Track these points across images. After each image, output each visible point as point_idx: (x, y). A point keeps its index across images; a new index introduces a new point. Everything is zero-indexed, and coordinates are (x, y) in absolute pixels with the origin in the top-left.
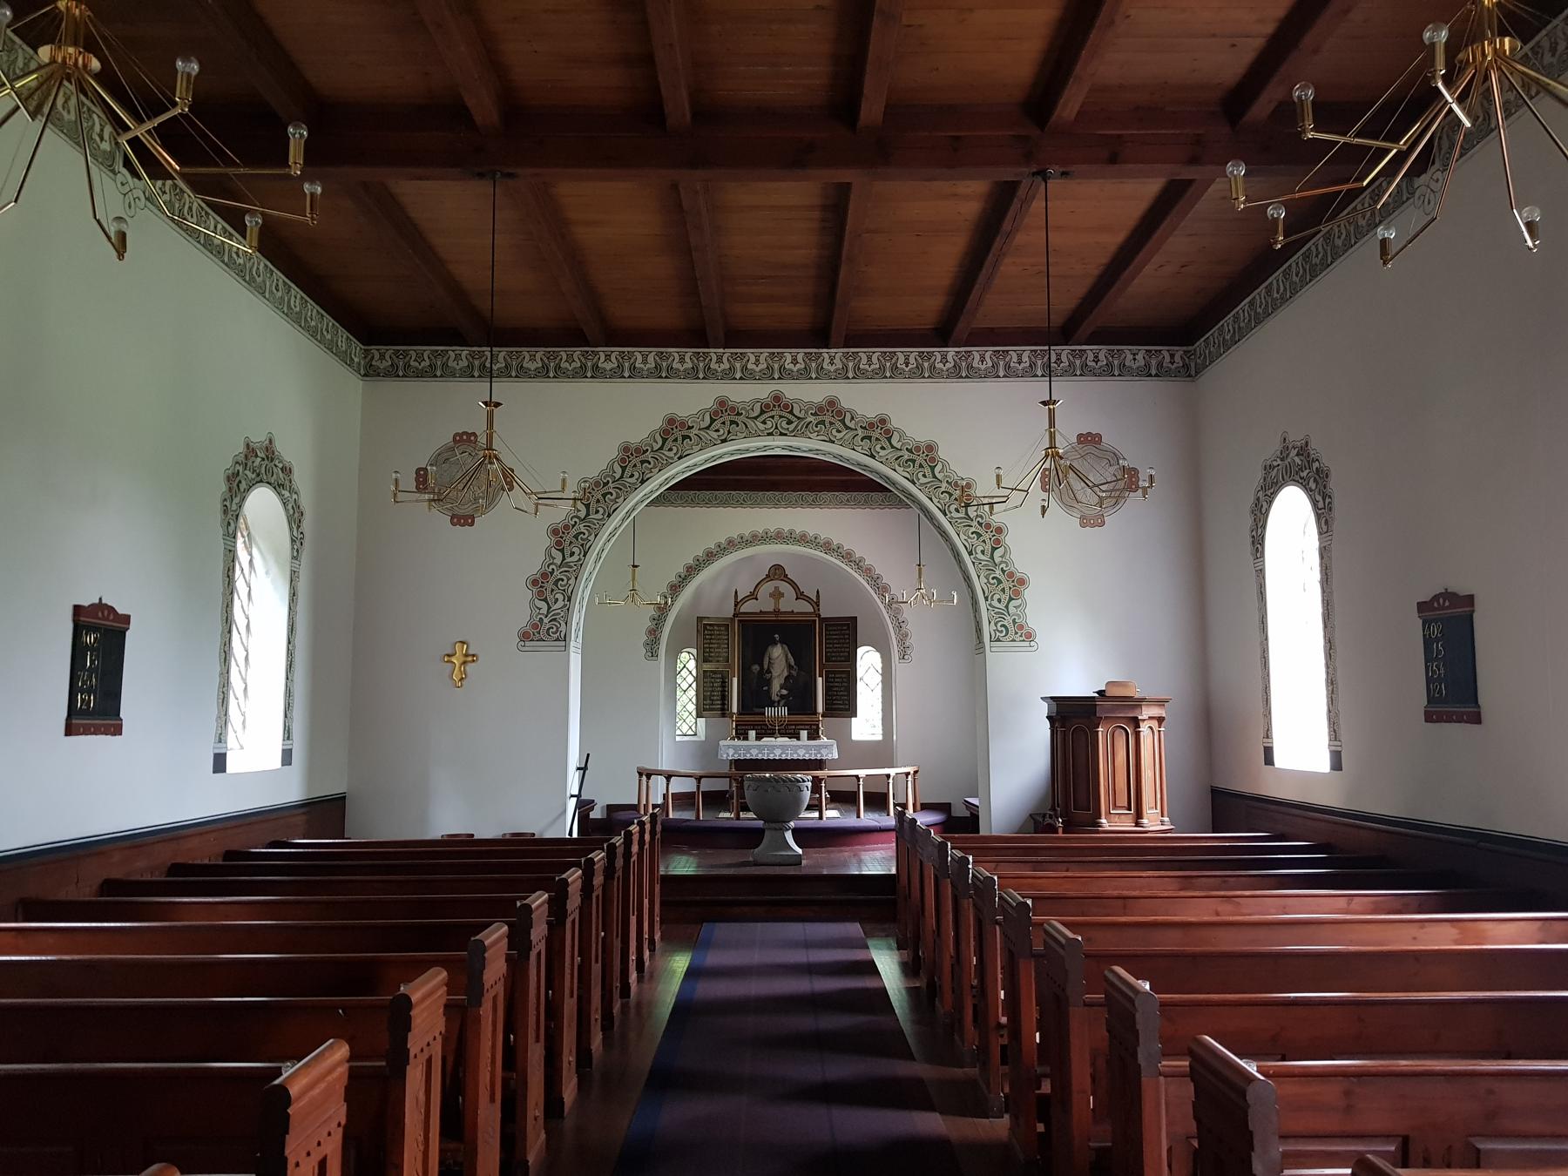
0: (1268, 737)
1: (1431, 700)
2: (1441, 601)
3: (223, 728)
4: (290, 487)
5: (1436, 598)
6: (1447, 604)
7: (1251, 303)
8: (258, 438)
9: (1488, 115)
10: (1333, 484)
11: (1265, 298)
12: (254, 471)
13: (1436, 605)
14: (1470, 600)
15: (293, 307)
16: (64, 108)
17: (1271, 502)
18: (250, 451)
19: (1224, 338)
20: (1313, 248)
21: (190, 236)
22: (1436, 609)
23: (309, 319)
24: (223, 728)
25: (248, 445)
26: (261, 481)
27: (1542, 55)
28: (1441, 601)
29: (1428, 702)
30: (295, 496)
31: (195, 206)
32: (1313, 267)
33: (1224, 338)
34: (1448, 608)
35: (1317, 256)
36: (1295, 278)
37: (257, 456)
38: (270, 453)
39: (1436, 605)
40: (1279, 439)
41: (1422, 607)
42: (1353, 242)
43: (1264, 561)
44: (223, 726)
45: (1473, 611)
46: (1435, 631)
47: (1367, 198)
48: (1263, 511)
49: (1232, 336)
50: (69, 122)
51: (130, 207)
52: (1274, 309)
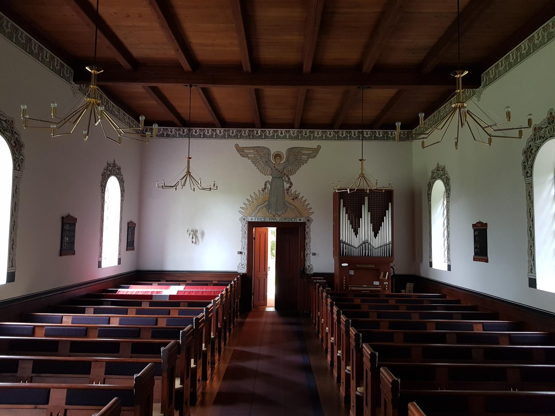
0: (532, 272)
1: (475, 254)
2: (478, 224)
3: (533, 267)
4: (120, 174)
5: (477, 223)
6: (480, 225)
7: (434, 116)
8: (111, 161)
9: (544, 37)
10: (451, 182)
11: (462, 95)
12: (110, 171)
13: (477, 225)
14: (486, 224)
15: (33, 49)
16: (20, 37)
17: (539, 147)
18: (109, 165)
19: (489, 77)
20: (500, 63)
21: (46, 66)
22: (477, 227)
23: (65, 73)
24: (533, 267)
25: (108, 163)
26: (112, 174)
27: (549, 28)
28: (478, 224)
29: (475, 255)
30: (122, 176)
31: (48, 54)
32: (466, 96)
33: (489, 77)
34: (480, 227)
35: (538, 39)
36: (511, 60)
37: (111, 166)
38: (114, 165)
39: (477, 225)
40: (436, 165)
41: (474, 226)
42: (532, 51)
43: (532, 179)
44: (533, 265)
45: (487, 228)
46: (477, 233)
47: (504, 60)
48: (533, 152)
49: (443, 114)
50: (36, 53)
51: (74, 93)
52: (510, 68)
